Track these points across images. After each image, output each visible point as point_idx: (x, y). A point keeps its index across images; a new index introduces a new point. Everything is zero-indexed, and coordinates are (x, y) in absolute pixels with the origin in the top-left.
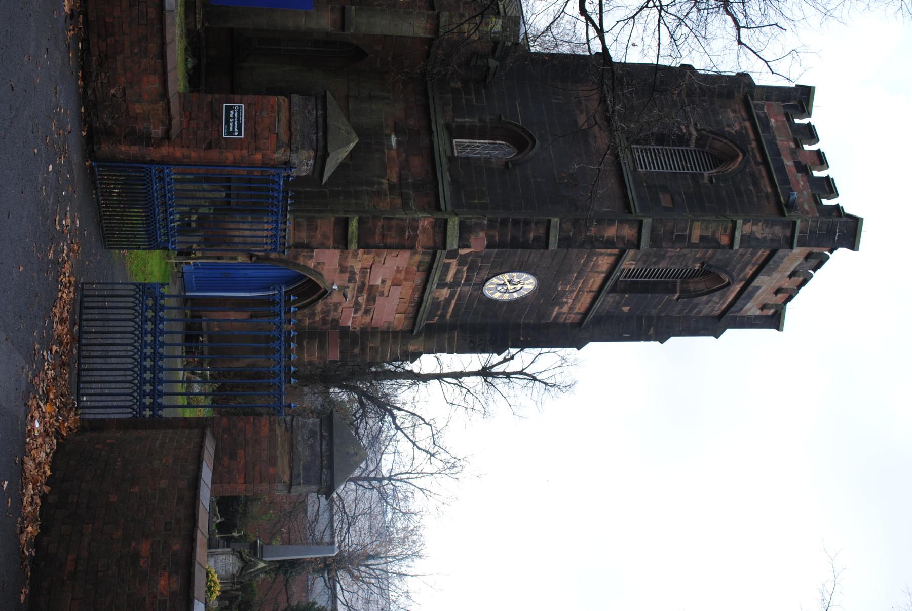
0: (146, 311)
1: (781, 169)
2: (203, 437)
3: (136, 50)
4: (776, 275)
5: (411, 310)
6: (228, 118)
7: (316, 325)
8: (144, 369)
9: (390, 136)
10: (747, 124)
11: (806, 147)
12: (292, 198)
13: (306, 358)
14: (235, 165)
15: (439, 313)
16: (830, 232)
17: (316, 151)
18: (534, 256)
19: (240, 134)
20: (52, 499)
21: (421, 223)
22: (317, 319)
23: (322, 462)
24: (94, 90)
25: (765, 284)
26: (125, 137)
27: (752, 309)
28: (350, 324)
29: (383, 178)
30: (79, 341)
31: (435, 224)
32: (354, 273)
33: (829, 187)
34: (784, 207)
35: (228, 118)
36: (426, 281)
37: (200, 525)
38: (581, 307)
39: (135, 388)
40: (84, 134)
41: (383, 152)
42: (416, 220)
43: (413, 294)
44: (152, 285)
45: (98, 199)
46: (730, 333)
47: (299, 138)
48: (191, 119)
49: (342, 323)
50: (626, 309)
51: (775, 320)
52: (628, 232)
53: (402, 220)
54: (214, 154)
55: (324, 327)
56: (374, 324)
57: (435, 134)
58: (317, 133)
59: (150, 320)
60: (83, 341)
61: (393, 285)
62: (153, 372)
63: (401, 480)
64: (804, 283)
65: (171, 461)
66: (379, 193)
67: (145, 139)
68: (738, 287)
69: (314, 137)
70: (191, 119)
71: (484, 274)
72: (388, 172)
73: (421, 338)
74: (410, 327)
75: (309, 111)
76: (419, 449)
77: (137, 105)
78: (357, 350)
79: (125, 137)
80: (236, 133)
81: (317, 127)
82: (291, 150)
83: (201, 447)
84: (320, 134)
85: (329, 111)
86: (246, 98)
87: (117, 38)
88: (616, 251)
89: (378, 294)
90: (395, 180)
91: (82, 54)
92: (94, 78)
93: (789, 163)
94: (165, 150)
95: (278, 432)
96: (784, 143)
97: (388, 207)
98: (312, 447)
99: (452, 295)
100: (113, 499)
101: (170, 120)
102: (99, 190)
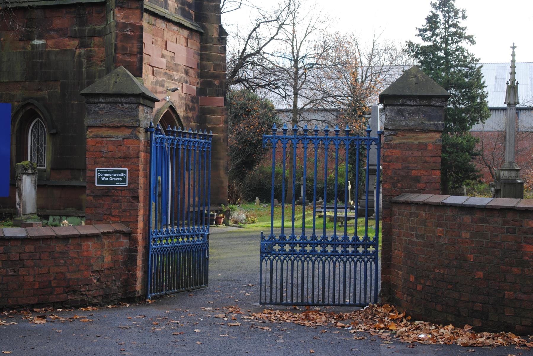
0: (285, 251)
2: (397, 203)
3: (62, 262)
6: (108, 182)
7: (195, 117)
8: (335, 252)
9: (33, 46)
12: (172, 128)
13: (222, 125)
15: (187, 9)
17: (139, 104)
19: (124, 172)
20: (478, 323)
21: (120, 20)
22: (190, 115)
23: (425, 105)
24: (94, 297)
26: (129, 271)
28: (195, 87)
29: (75, 53)
30: (310, 305)
31: (121, 7)
32: (157, 81)
35: (108, 182)
36: (163, 18)
37: (513, 205)
39: (287, 259)
40: (128, 305)
41: (49, 51)
42: (117, 25)
43: (173, 31)
44: (262, 246)
45: (174, 293)
47: (127, 120)
48: (110, 214)
49: (194, 94)
53: (117, 37)
54: (141, 194)
55: (197, 109)
56: (195, 66)
57: (31, 4)
58: (122, 103)
59: (293, 248)
60: (310, 302)
61: (166, 48)
62: (295, 244)
63: (298, 52)
65: (441, 229)
66: (89, 57)
67: (131, 253)
69: (126, 106)
70: (110, 214)
72: (68, 48)
73: (207, 25)
74: (198, 35)
75: (100, 110)
76: (277, 34)
77: (106, 260)
78: (217, 82)
79: (129, 271)
80: (123, 175)
81: (116, 103)
82: (139, 126)
83: (419, 205)
84: (123, 100)
85: (101, 91)
86: (89, 166)
87: (52, 278)
89: (173, 62)
90: (76, 42)
91: (66, 308)
92: (85, 298)
94: (140, 237)
95: (397, 142)
97: (103, 49)
98: (411, 114)
100: (480, 275)
101: (117, 232)
102: (167, 292)
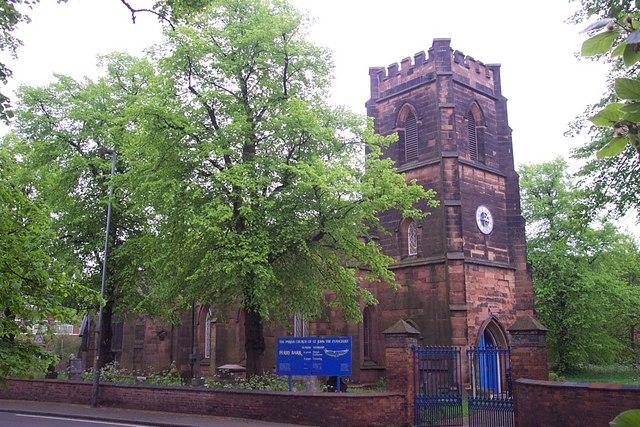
1: (412, 82)
2: (516, 383)
4: (469, 76)
5: (502, 272)
10: (391, 101)
11: (400, 69)
14: (414, 369)
16: (442, 55)
18: (465, 211)
25: (474, 80)
27: (490, 84)
33: (419, 57)
34: (430, 79)
38: (494, 179)
46: (505, 93)
50: (494, 153)
51: (495, 69)
52: (449, 163)
64: (472, 60)
68: (477, 95)
71: (478, 235)
88: (460, 167)
93: (409, 78)
96: (399, 80)
99: (492, 250)
